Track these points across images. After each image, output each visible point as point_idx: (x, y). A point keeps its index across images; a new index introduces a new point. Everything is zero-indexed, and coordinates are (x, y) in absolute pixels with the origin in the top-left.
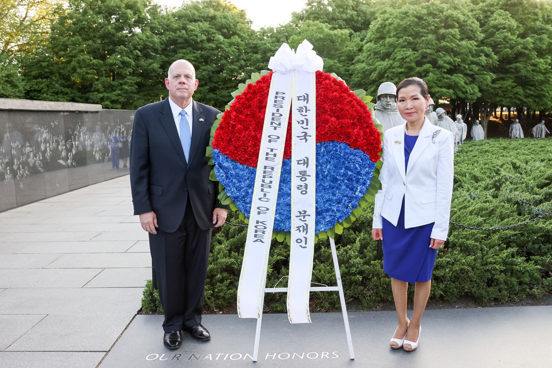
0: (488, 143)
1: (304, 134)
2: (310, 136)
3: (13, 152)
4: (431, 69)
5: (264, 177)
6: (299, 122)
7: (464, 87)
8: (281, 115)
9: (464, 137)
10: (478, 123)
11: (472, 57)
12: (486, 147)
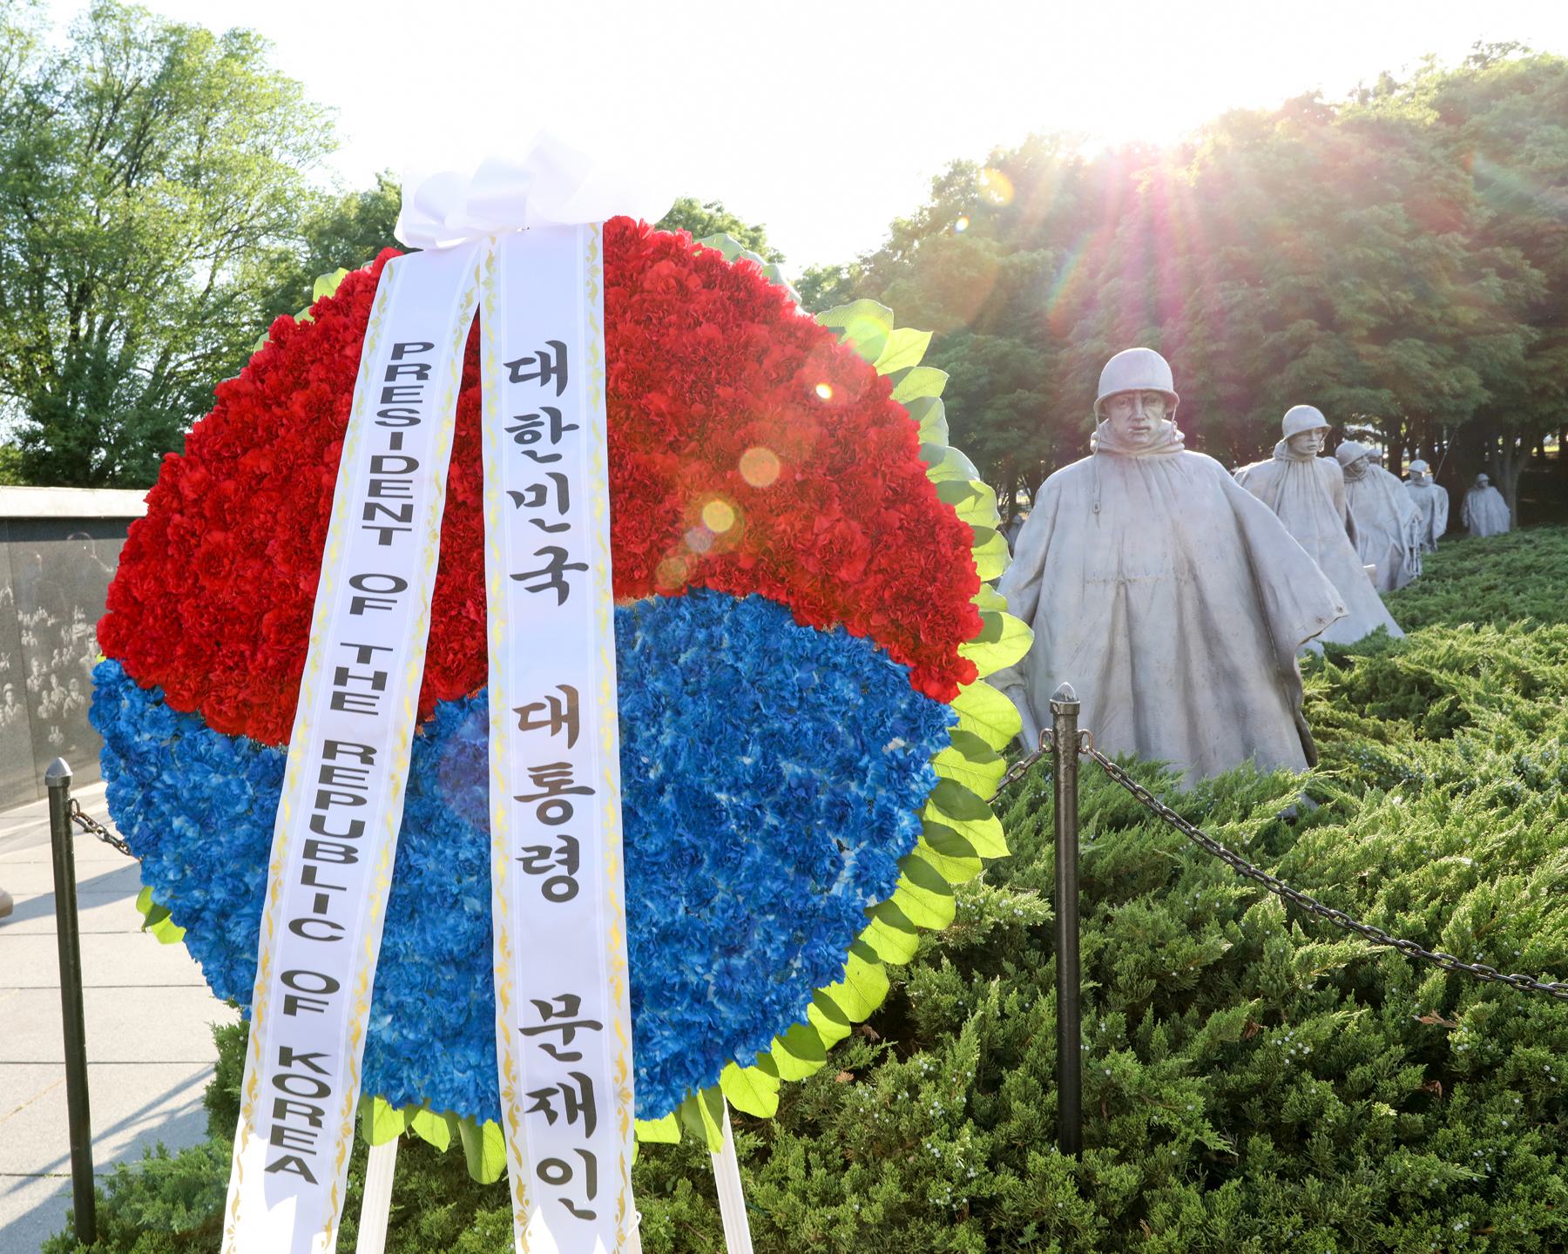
0: (1530, 542)
1: (549, 558)
2: (583, 567)
3: (24, 640)
4: (1316, 334)
5: (323, 800)
6: (518, 498)
7: (1429, 378)
8: (412, 465)
9: (1440, 527)
10: (1485, 484)
11: (1453, 283)
12: (1524, 556)
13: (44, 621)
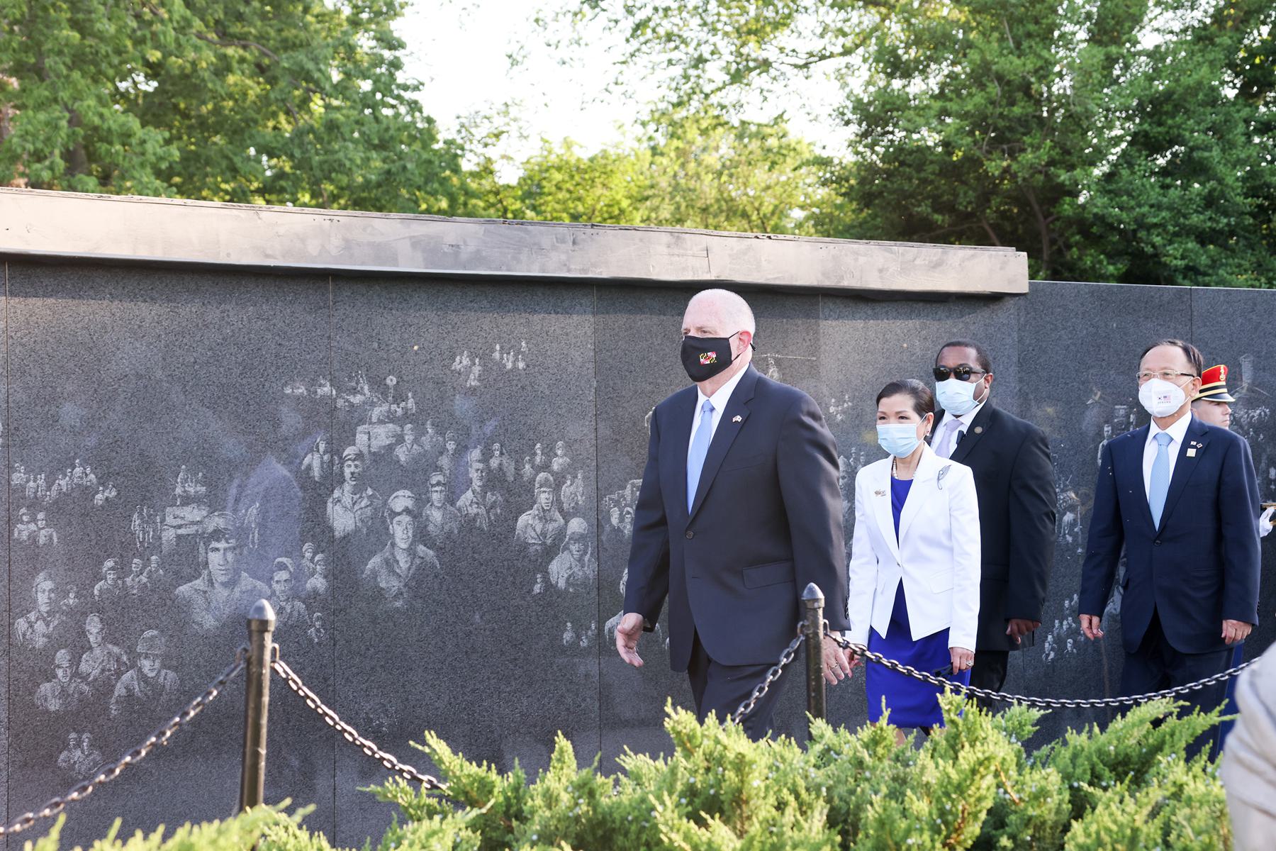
13: (87, 493)
